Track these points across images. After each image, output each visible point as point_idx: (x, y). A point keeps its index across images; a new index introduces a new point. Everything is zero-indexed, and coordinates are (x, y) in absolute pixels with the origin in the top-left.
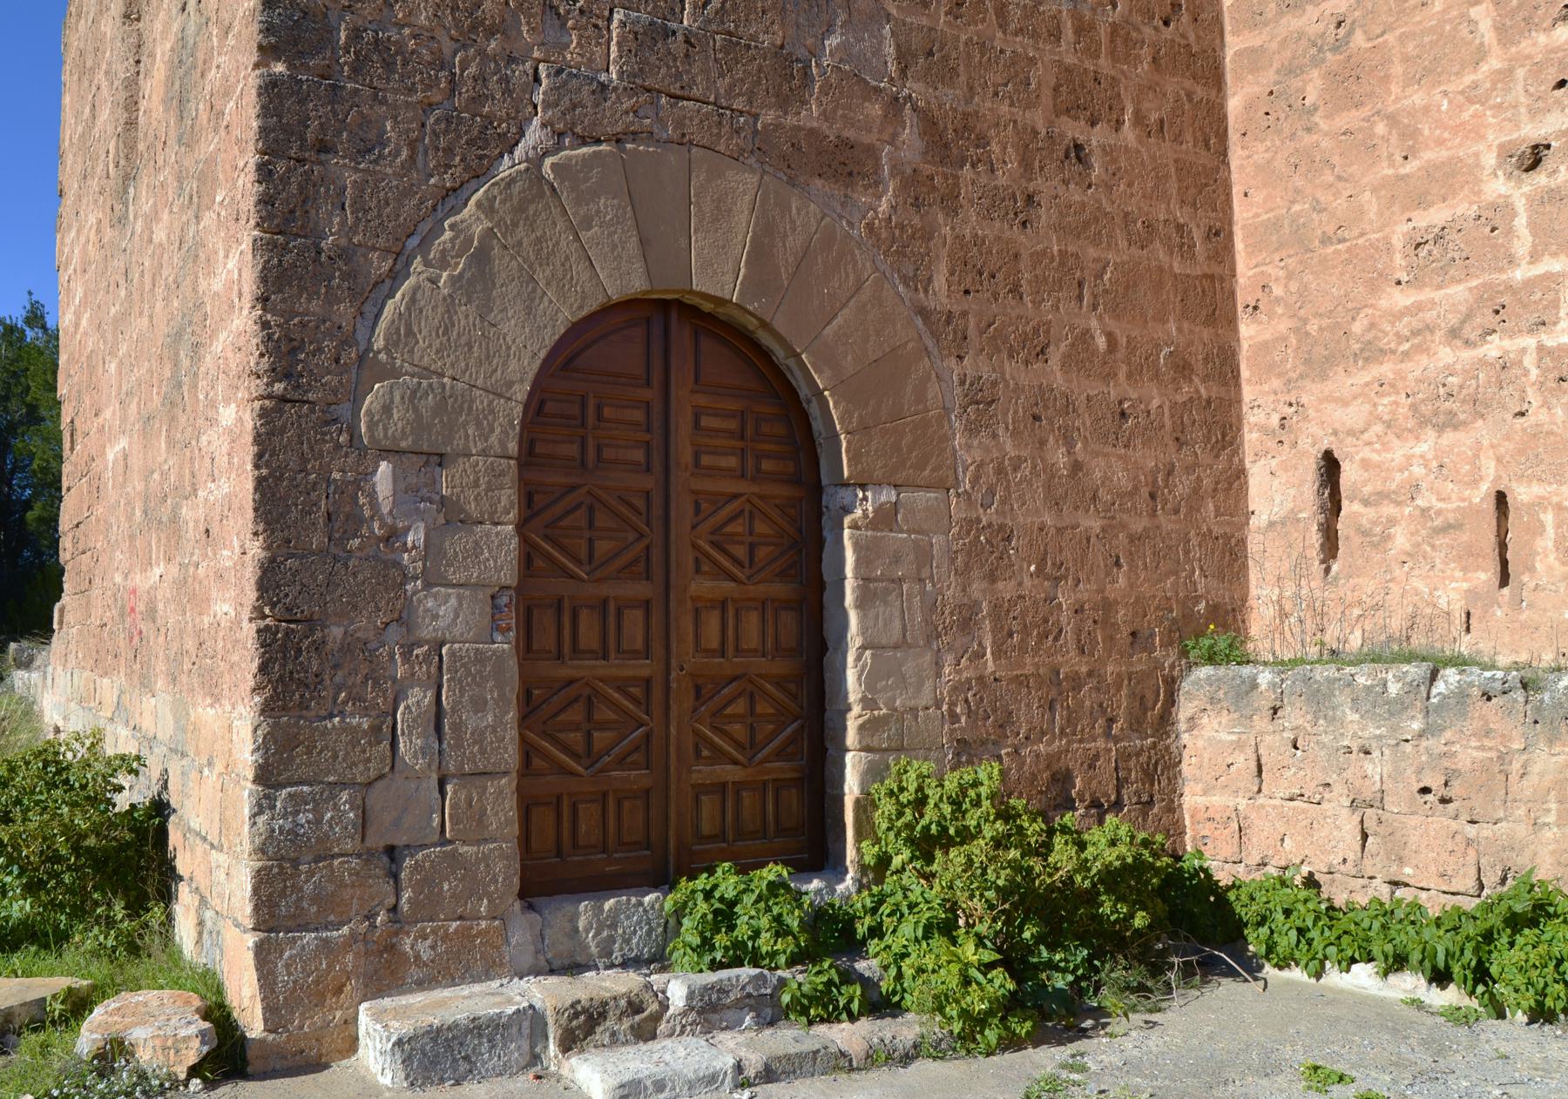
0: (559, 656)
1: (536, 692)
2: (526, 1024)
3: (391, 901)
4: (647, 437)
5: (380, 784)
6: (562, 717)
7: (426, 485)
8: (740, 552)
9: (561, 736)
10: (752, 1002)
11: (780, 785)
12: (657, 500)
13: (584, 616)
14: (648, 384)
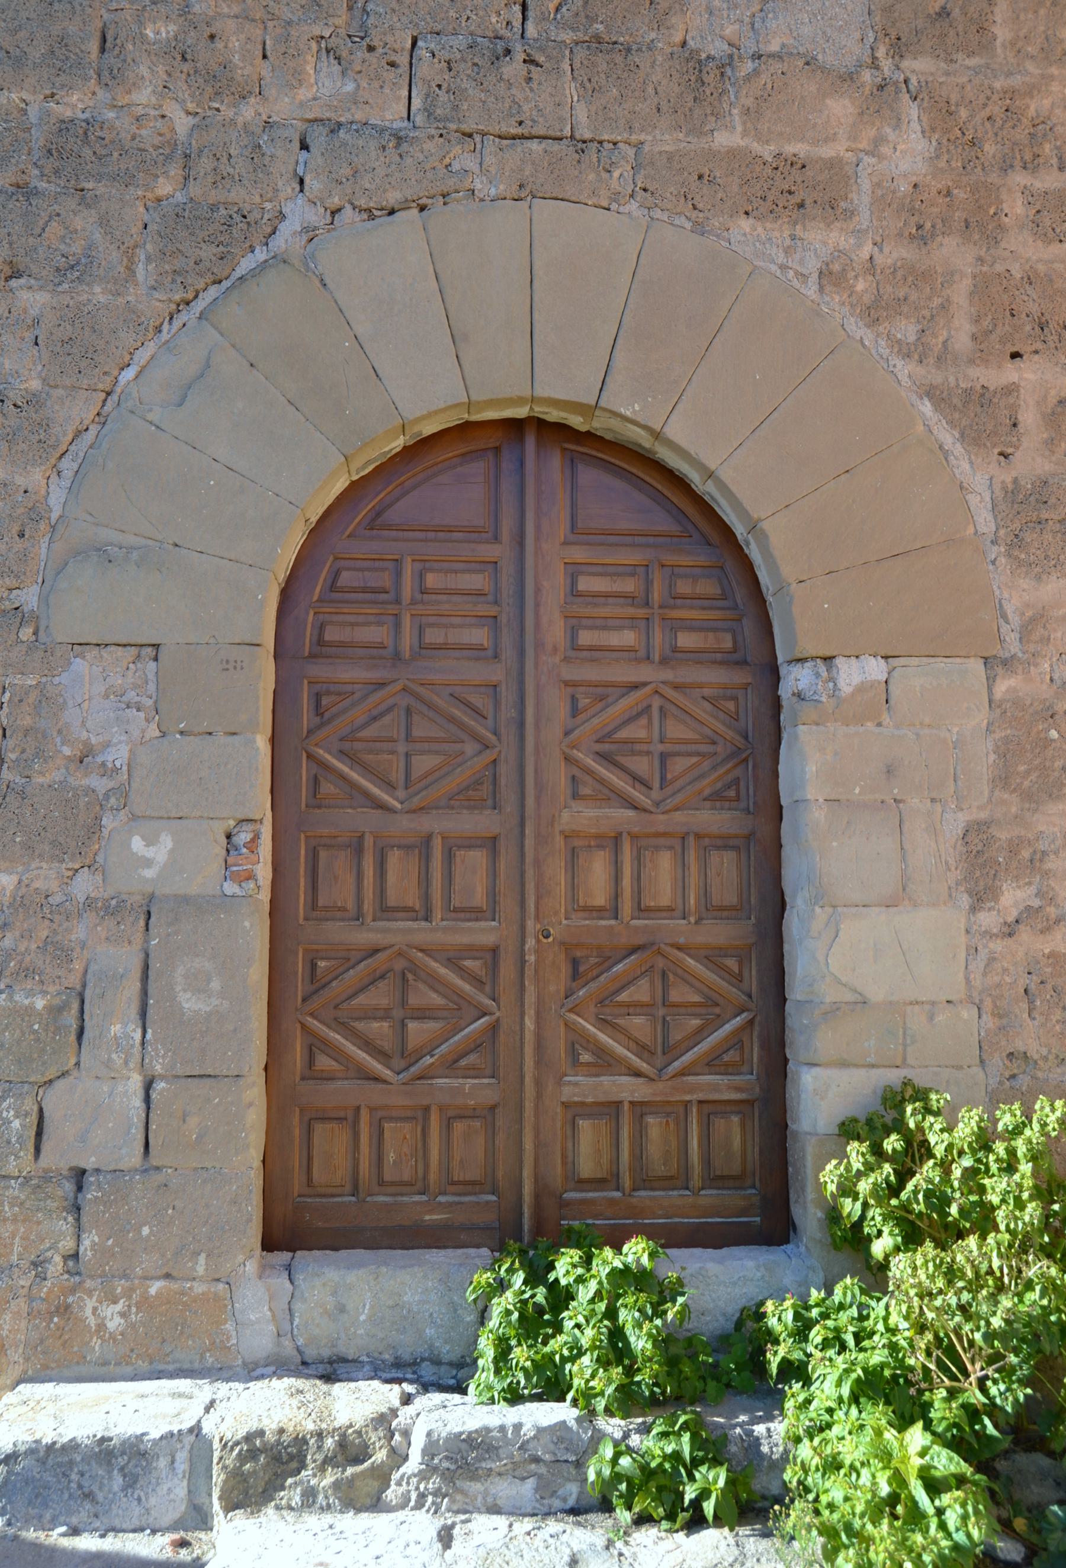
0: (359, 916)
1: (322, 964)
2: (182, 1456)
3: (67, 1244)
4: (492, 611)
5: (60, 1085)
6: (361, 1000)
7: (135, 686)
8: (641, 765)
9: (360, 1026)
10: (542, 1470)
11: (711, 1110)
12: (507, 696)
13: (394, 858)
14: (496, 539)
